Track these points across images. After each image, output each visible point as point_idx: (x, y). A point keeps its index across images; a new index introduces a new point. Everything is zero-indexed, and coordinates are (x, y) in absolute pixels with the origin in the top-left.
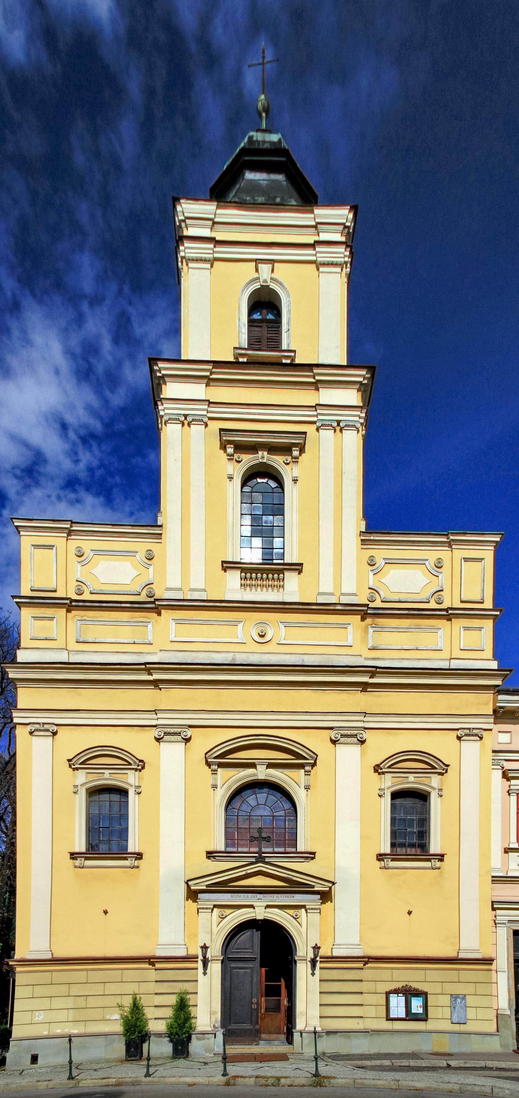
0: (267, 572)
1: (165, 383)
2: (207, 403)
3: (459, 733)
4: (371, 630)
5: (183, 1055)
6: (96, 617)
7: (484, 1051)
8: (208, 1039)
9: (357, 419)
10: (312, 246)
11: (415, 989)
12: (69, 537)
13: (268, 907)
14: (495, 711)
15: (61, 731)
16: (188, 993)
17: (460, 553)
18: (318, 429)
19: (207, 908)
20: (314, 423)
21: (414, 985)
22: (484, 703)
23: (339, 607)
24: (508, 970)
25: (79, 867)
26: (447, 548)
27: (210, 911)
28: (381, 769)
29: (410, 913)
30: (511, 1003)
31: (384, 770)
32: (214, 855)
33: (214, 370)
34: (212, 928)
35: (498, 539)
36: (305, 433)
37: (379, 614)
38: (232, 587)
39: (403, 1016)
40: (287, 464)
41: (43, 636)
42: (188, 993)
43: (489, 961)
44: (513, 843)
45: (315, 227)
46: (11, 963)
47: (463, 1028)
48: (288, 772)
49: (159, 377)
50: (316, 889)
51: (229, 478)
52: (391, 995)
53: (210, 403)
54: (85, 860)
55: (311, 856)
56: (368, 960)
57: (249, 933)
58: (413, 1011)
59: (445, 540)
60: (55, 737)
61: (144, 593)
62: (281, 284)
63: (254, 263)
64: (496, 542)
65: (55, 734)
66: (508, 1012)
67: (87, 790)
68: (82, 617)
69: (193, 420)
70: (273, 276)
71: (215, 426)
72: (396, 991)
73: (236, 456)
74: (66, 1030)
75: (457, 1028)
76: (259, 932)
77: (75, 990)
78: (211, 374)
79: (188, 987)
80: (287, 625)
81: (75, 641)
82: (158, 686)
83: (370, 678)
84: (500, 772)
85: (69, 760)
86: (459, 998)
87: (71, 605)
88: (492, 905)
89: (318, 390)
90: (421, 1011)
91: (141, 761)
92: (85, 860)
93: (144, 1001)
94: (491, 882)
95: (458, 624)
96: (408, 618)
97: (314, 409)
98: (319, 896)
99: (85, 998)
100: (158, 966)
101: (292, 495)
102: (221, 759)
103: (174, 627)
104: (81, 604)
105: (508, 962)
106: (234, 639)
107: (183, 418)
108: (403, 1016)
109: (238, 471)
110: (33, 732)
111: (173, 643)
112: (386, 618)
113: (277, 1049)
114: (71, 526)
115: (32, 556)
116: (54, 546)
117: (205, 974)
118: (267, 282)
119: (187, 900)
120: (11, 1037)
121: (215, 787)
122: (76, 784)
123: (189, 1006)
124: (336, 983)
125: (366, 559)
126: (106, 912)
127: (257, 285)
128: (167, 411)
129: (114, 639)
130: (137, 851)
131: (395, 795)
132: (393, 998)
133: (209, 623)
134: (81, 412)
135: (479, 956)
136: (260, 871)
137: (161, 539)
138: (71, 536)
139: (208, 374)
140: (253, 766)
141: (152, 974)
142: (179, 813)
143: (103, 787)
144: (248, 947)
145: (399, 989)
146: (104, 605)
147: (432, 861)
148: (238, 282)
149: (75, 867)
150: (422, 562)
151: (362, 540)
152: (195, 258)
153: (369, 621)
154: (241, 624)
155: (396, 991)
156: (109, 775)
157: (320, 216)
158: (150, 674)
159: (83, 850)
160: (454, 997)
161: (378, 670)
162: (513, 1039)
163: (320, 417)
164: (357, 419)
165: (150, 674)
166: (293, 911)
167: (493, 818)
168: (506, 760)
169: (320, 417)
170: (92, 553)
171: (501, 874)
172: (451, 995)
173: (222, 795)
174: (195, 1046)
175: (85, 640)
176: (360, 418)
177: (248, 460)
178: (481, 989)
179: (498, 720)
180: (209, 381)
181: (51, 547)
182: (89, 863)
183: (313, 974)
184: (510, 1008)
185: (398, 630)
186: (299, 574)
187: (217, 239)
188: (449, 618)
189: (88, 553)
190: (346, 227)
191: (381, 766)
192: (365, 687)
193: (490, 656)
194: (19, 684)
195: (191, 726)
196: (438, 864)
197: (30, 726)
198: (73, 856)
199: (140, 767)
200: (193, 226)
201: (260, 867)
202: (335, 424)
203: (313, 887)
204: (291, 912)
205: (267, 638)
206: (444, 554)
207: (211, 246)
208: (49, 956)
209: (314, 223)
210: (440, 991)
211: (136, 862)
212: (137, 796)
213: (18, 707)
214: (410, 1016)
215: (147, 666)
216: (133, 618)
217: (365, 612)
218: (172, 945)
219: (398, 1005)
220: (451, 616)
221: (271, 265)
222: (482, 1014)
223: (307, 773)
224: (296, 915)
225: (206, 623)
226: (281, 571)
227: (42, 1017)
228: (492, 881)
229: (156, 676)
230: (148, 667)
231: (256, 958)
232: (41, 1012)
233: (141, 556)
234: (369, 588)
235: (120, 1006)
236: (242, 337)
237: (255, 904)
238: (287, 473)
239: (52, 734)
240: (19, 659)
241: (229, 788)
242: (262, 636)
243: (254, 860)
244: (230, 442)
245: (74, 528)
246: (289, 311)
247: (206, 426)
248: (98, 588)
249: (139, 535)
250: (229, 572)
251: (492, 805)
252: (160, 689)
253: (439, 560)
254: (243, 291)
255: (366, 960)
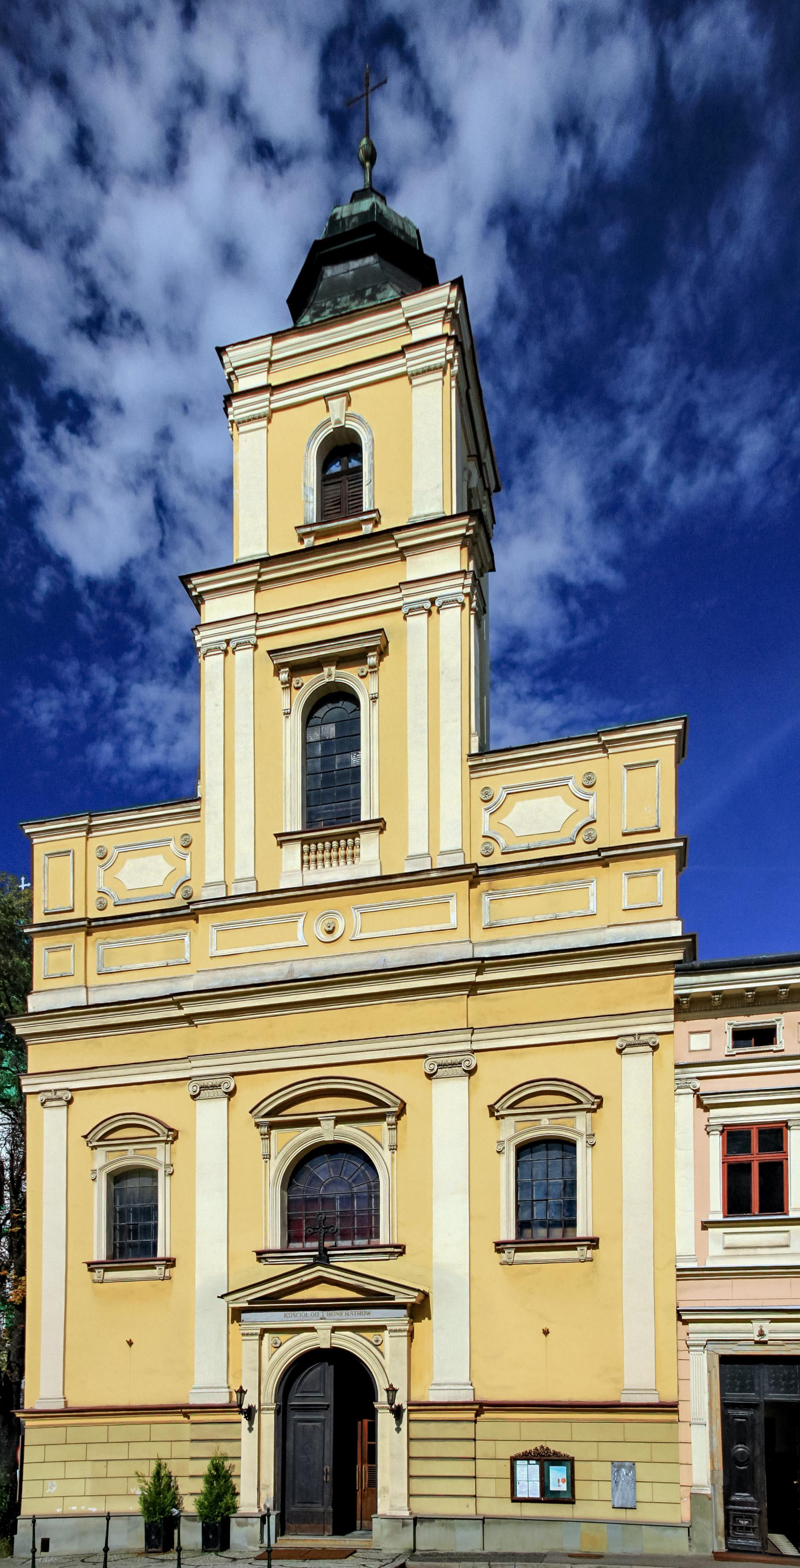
0: (338, 838)
1: (203, 602)
2: (255, 617)
3: (618, 1043)
4: (486, 899)
5: (215, 1547)
6: (122, 937)
7: (662, 1553)
8: (253, 1525)
9: (460, 589)
10: (401, 353)
11: (555, 1453)
12: (90, 835)
13: (334, 1329)
14: (677, 1001)
15: (77, 1096)
16: (226, 1458)
17: (619, 758)
18: (405, 618)
19: (252, 1334)
20: (398, 609)
21: (553, 1447)
22: (665, 988)
23: (434, 875)
24: (711, 1422)
25: (98, 1282)
26: (601, 755)
27: (257, 1337)
28: (498, 1111)
29: (546, 1332)
30: (716, 1475)
31: (502, 1113)
32: (264, 1256)
33: (263, 570)
34: (258, 1364)
35: (680, 727)
36: (381, 630)
37: (495, 873)
38: (290, 868)
39: (537, 1495)
40: (363, 677)
41: (58, 972)
42: (226, 1458)
43: (671, 1408)
44: (715, 1212)
45: (406, 324)
46: (18, 1415)
47: (630, 1515)
48: (364, 1126)
49: (196, 596)
50: (397, 1301)
51: (285, 714)
52: (518, 1462)
53: (258, 616)
54: (105, 1271)
55: (399, 1250)
56: (481, 1407)
57: (319, 1368)
58: (552, 1488)
59: (596, 743)
60: (71, 1106)
61: (179, 895)
62: (359, 419)
63: (323, 401)
64: (678, 730)
65: (70, 1102)
66: (708, 1491)
67: (109, 1175)
68: (105, 939)
69: (238, 645)
70: (350, 410)
71: (266, 645)
72: (526, 1456)
73: (294, 683)
74: (83, 1508)
75: (621, 1515)
76: (332, 1366)
77: (95, 1452)
78: (259, 576)
79: (225, 1449)
80: (364, 912)
81: (96, 972)
82: (193, 1023)
83: (477, 975)
84: (691, 1100)
85: (85, 1137)
86: (624, 1467)
87: (90, 926)
88: (679, 1317)
89: (405, 560)
90: (564, 1487)
91: (597, 1097)
92: (105, 1271)
93: (173, 1467)
94: (675, 1278)
95: (620, 869)
96: (541, 873)
97: (398, 590)
98: (404, 1312)
99: (105, 1463)
100: (194, 1418)
101: (370, 719)
102: (275, 1117)
103: (214, 937)
104: (102, 923)
105: (710, 1408)
106: (294, 943)
107: (224, 646)
108: (537, 1495)
109: (299, 699)
110: (45, 1102)
111: (214, 959)
112: (507, 877)
113: (352, 1543)
114: (91, 821)
115: (45, 868)
116: (69, 851)
117: (250, 1429)
118: (340, 423)
119: (232, 1323)
120: (19, 1514)
121: (267, 1157)
122: (501, 1139)
123: (231, 1476)
124: (435, 1443)
125: (477, 795)
126: (130, 1343)
127: (329, 430)
128: (204, 641)
129: (141, 965)
130: (590, 1235)
131: (524, 1149)
132: (522, 1467)
133: (260, 923)
134: (593, 561)
135: (654, 1399)
136: (320, 1277)
137: (199, 816)
138: (91, 833)
139: (255, 577)
140: (316, 1122)
141: (186, 1431)
142: (222, 1204)
143: (299, 1159)
144: (317, 1388)
145: (530, 1453)
146: (129, 919)
147: (578, 1248)
148: (302, 431)
149: (94, 1282)
150: (562, 783)
151: (471, 767)
152: (246, 419)
153: (483, 885)
154: (302, 919)
155: (526, 1456)
156: (547, 1122)
157: (409, 309)
158: (181, 1008)
159: (103, 1258)
160: (617, 1466)
161: (486, 962)
162: (717, 1534)
163: (407, 600)
164: (460, 589)
165: (180, 1008)
166: (373, 1334)
167: (678, 1174)
168: (699, 1078)
169: (407, 600)
170: (116, 852)
171: (694, 1265)
172: (612, 1462)
173: (277, 1167)
174: (238, 1534)
175: (109, 970)
176: (464, 586)
177: (310, 682)
178: (660, 1452)
179: (682, 1016)
180: (258, 586)
181: (67, 853)
182: (110, 1275)
183: (398, 1430)
184: (713, 1485)
185: (528, 893)
186: (381, 832)
187: (273, 384)
188: (604, 862)
189: (113, 853)
190: (446, 310)
191: (496, 1107)
192: (472, 988)
193: (673, 915)
194: (28, 1041)
195: (234, 1075)
196: (589, 1253)
197: (619, 1040)
198: (92, 1266)
199: (170, 1139)
200: (245, 375)
201: (320, 1271)
202: (428, 605)
203: (393, 1298)
204: (370, 1335)
205: (337, 934)
206: (595, 763)
207: (267, 395)
208: (61, 1406)
209: (403, 320)
210: (594, 1457)
211: (167, 1270)
212: (590, 1150)
213: (29, 1072)
214: (548, 1496)
215: (175, 998)
216: (165, 931)
217: (473, 875)
218: (211, 1388)
219: (528, 1478)
220: (607, 860)
221: (345, 398)
222: (663, 1493)
223: (393, 1127)
224: (377, 1341)
225: (255, 924)
226: (356, 834)
227: (54, 1489)
228: (678, 1276)
229: (187, 1010)
230: (176, 999)
231: (328, 1406)
232: (54, 1482)
233: (174, 847)
234: (484, 836)
235: (138, 1476)
236: (306, 504)
237: (316, 1326)
238: (363, 690)
239: (651, 1049)
240: (31, 1009)
241: (286, 1157)
242: (330, 932)
243: (311, 1261)
244: (284, 665)
245: (94, 823)
246: (372, 455)
247: (256, 646)
248: (124, 896)
249: (113, 826)
250: (285, 846)
251: (677, 1152)
252: (196, 1026)
253: (589, 775)
254: (309, 444)
255: (477, 1407)
